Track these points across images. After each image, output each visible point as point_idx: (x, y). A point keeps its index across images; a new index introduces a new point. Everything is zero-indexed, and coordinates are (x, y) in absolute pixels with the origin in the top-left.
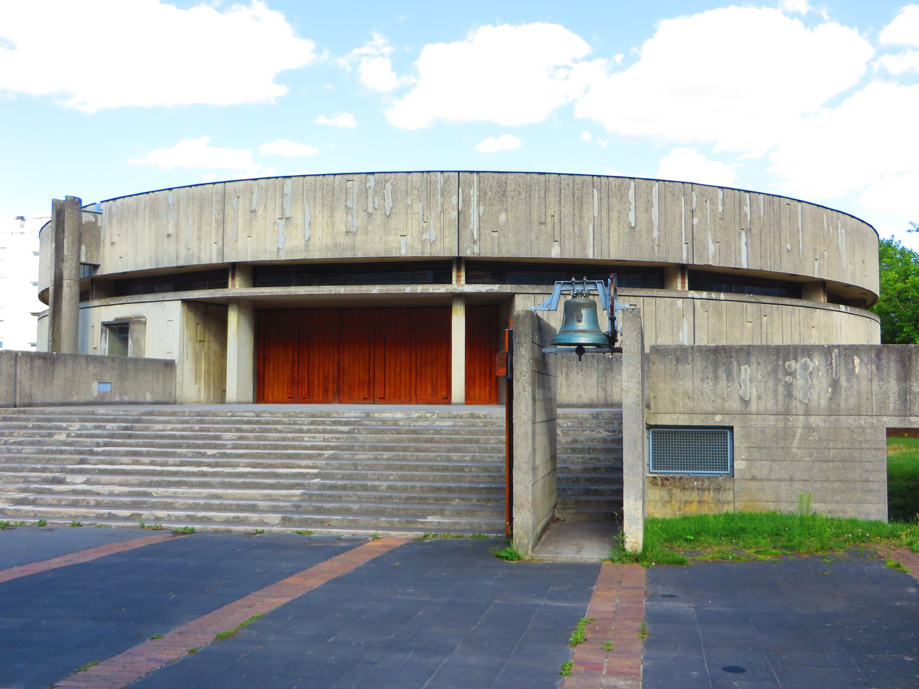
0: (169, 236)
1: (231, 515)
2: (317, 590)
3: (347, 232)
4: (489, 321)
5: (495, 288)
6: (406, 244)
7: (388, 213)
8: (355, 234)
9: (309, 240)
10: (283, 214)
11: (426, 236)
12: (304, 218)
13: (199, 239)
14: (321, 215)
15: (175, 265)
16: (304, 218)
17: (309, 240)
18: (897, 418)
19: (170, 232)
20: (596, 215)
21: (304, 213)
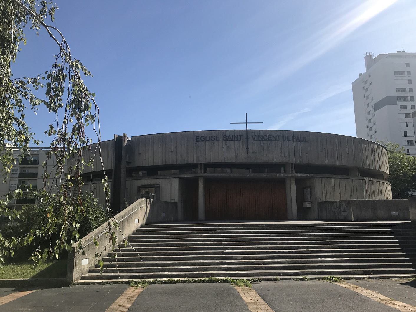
0: (172, 151)
1: (224, 278)
2: (112, 303)
3: (253, 152)
4: (303, 187)
5: (304, 175)
6: (276, 157)
7: (268, 146)
8: (256, 153)
9: (237, 155)
10: (226, 145)
11: (283, 155)
12: (235, 146)
13: (188, 153)
14: (242, 145)
15: (142, 166)
16: (235, 146)
17: (237, 155)
18: (133, 224)
19: (173, 150)
20: (338, 149)
21: (235, 144)
